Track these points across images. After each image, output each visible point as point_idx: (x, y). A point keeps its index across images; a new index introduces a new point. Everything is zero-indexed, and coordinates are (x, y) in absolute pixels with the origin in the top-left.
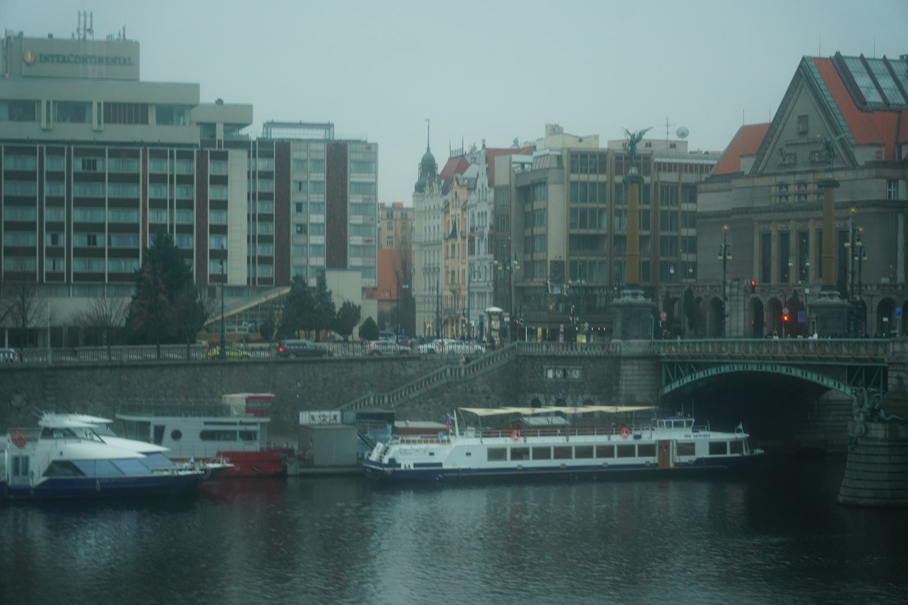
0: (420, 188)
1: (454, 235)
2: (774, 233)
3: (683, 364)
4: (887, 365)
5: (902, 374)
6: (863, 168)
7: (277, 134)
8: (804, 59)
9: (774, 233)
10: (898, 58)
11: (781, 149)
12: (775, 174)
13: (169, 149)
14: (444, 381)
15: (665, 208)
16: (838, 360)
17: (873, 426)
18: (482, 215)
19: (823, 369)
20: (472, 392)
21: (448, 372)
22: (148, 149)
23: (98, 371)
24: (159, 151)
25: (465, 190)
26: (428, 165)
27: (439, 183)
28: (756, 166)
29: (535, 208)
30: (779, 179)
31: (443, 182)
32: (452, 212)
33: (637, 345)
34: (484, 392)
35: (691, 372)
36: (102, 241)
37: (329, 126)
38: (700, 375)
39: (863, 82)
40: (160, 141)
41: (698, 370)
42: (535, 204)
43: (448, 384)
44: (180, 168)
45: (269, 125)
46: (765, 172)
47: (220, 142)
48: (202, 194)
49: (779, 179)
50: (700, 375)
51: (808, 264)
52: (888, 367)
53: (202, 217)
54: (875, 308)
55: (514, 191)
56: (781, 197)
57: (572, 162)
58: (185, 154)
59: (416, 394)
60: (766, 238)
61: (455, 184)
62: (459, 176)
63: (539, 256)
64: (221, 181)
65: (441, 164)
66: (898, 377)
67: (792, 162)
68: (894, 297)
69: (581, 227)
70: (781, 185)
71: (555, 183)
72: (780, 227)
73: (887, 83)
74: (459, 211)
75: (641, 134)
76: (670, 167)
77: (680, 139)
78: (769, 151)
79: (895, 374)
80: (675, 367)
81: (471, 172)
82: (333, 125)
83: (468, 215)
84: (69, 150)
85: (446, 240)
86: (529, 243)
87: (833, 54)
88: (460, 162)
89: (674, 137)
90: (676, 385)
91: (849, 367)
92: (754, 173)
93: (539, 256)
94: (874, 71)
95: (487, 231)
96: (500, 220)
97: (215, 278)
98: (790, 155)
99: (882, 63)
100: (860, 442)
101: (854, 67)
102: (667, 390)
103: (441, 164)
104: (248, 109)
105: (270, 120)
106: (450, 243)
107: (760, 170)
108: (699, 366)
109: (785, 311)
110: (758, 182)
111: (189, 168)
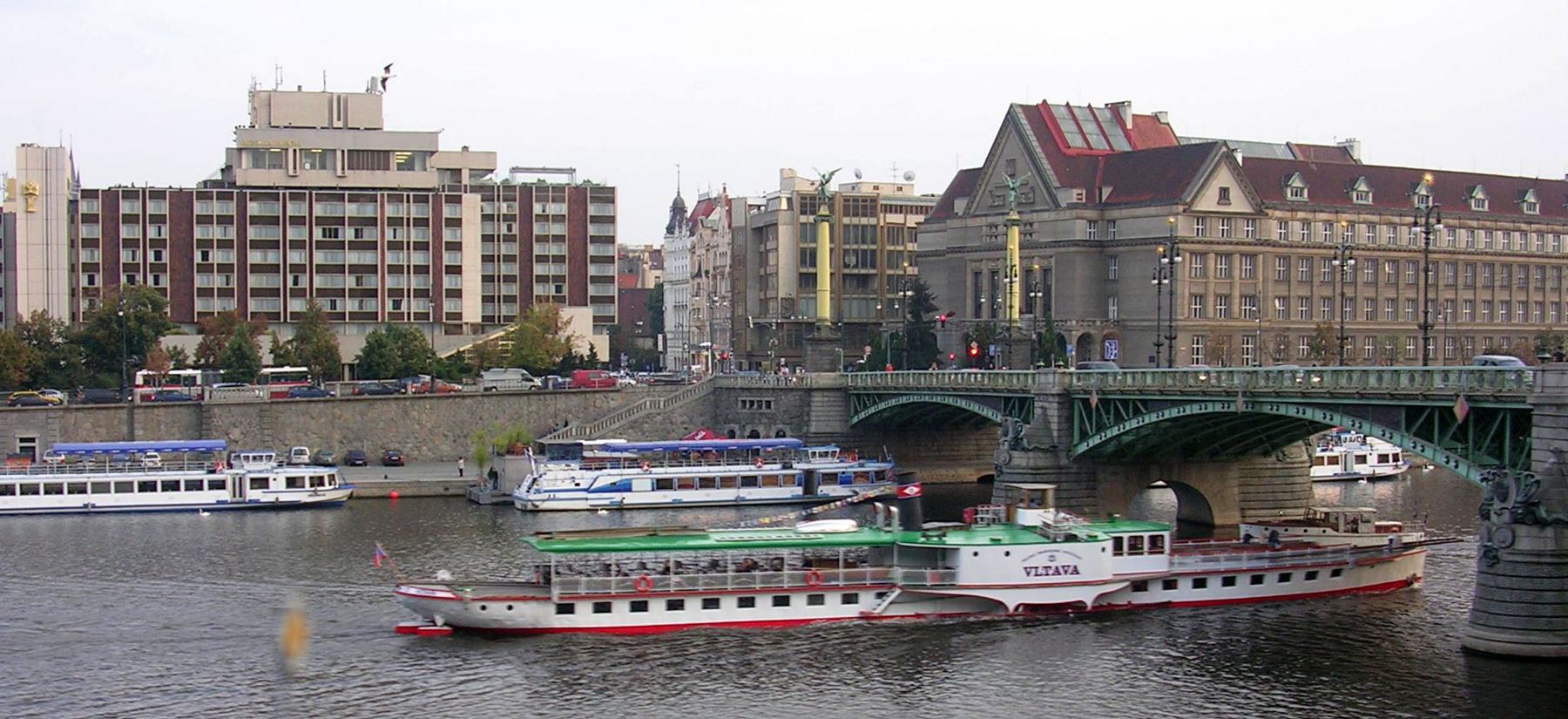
0: (670, 230)
1: (699, 275)
2: (985, 271)
3: (1125, 403)
4: (1531, 407)
5: (1046, 405)
6: (1064, 209)
7: (521, 179)
8: (1011, 106)
9: (985, 271)
10: (1103, 106)
11: (991, 192)
12: (986, 215)
13: (405, 193)
14: (643, 413)
15: (892, 248)
16: (995, 391)
17: (1015, 454)
18: (724, 254)
19: (983, 400)
20: (671, 423)
21: (648, 403)
22: (314, 192)
23: (313, 405)
24: (396, 195)
25: (709, 232)
26: (678, 208)
27: (687, 225)
28: (968, 208)
29: (768, 248)
30: (990, 220)
31: (690, 224)
32: (698, 253)
33: (826, 379)
34: (683, 423)
35: (1137, 412)
36: (350, 282)
37: (571, 171)
38: (882, 406)
39: (1067, 127)
40: (136, 186)
41: (881, 401)
42: (768, 244)
43: (648, 416)
44: (415, 211)
45: (515, 170)
46: (976, 213)
47: (466, 186)
48: (438, 235)
49: (990, 220)
50: (882, 406)
51: (983, 300)
52: (1532, 410)
53: (438, 257)
54: (1074, 341)
55: (749, 231)
56: (991, 237)
57: (803, 206)
58: (421, 196)
59: (617, 425)
60: (977, 274)
61: (700, 225)
62: (703, 217)
63: (770, 294)
64: (456, 223)
65: (690, 206)
66: (1042, 407)
67: (1001, 203)
68: (1092, 332)
69: (862, 267)
70: (990, 226)
71: (785, 224)
72: (992, 265)
73: (1090, 128)
74: (704, 252)
75: (825, 182)
76: (899, 209)
77: (906, 182)
78: (980, 192)
79: (1041, 404)
80: (1112, 407)
81: (714, 216)
82: (575, 170)
83: (711, 256)
84: (311, 194)
85: (693, 278)
86: (765, 281)
87: (1040, 102)
88: (707, 205)
89: (901, 181)
90: (862, 415)
91: (1005, 397)
92: (966, 215)
93: (770, 294)
94: (1072, 122)
95: (727, 269)
96: (738, 261)
97: (450, 316)
98: (999, 196)
99: (1088, 111)
100: (1005, 470)
101: (1061, 114)
102: (855, 420)
103: (690, 206)
104: (491, 155)
105: (515, 166)
106: (695, 283)
107: (972, 211)
108: (881, 398)
109: (974, 345)
110: (970, 222)
111: (427, 211)
